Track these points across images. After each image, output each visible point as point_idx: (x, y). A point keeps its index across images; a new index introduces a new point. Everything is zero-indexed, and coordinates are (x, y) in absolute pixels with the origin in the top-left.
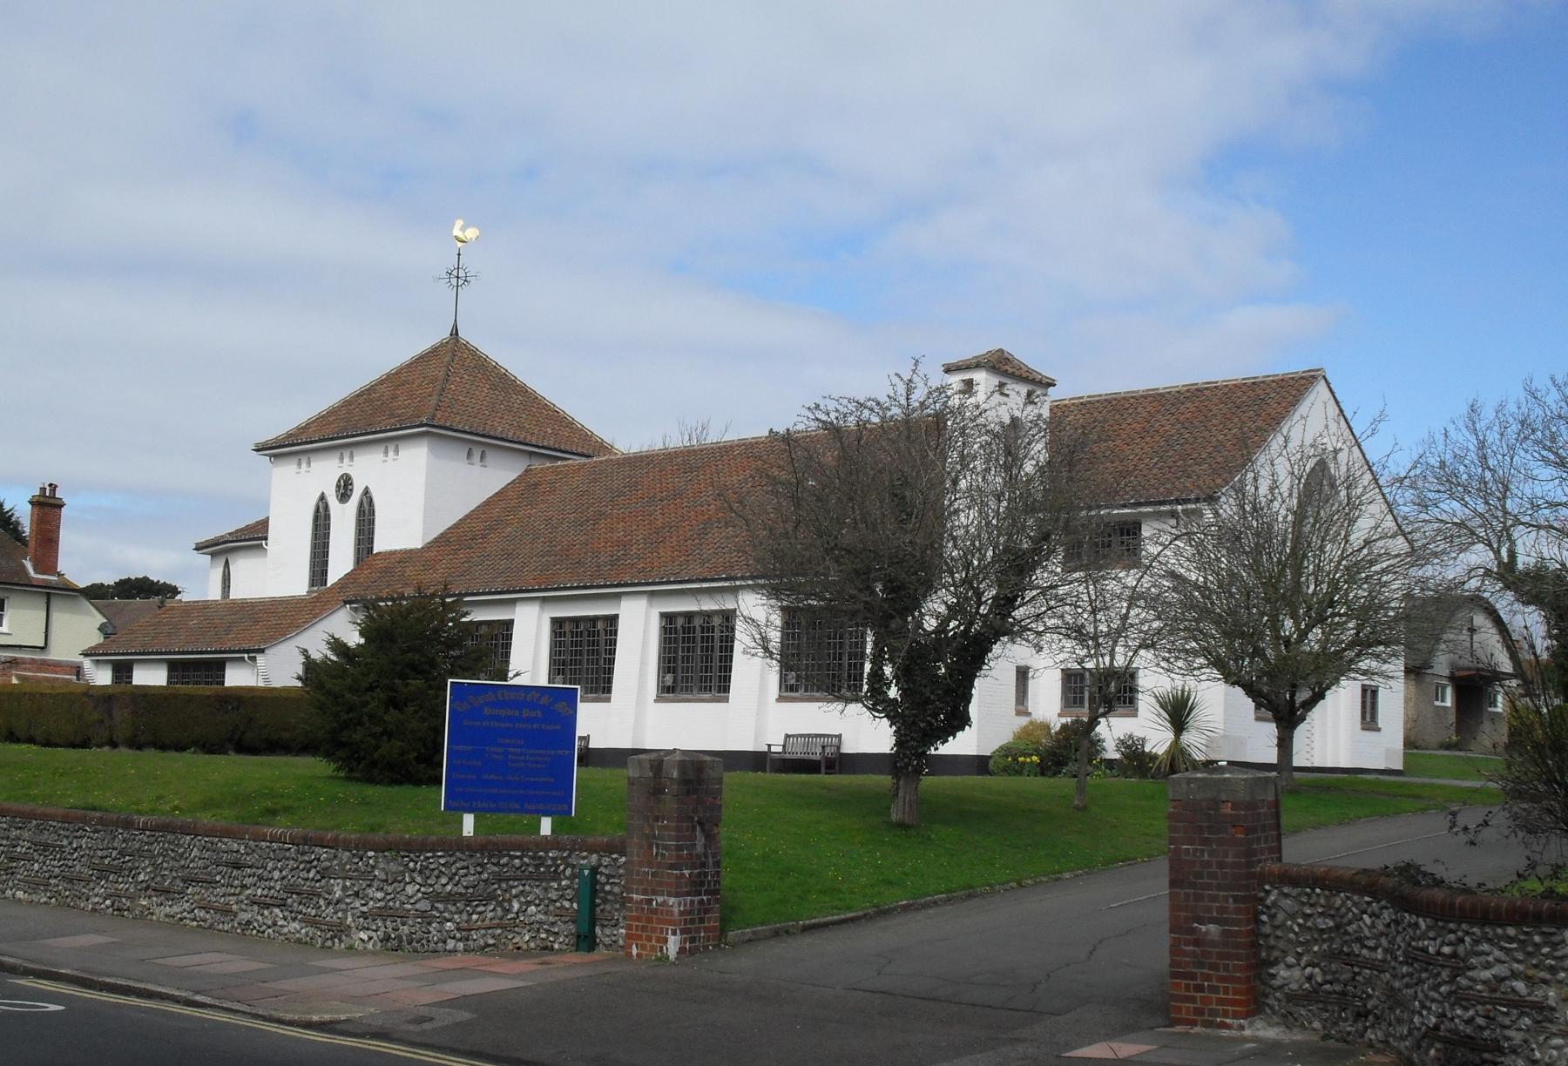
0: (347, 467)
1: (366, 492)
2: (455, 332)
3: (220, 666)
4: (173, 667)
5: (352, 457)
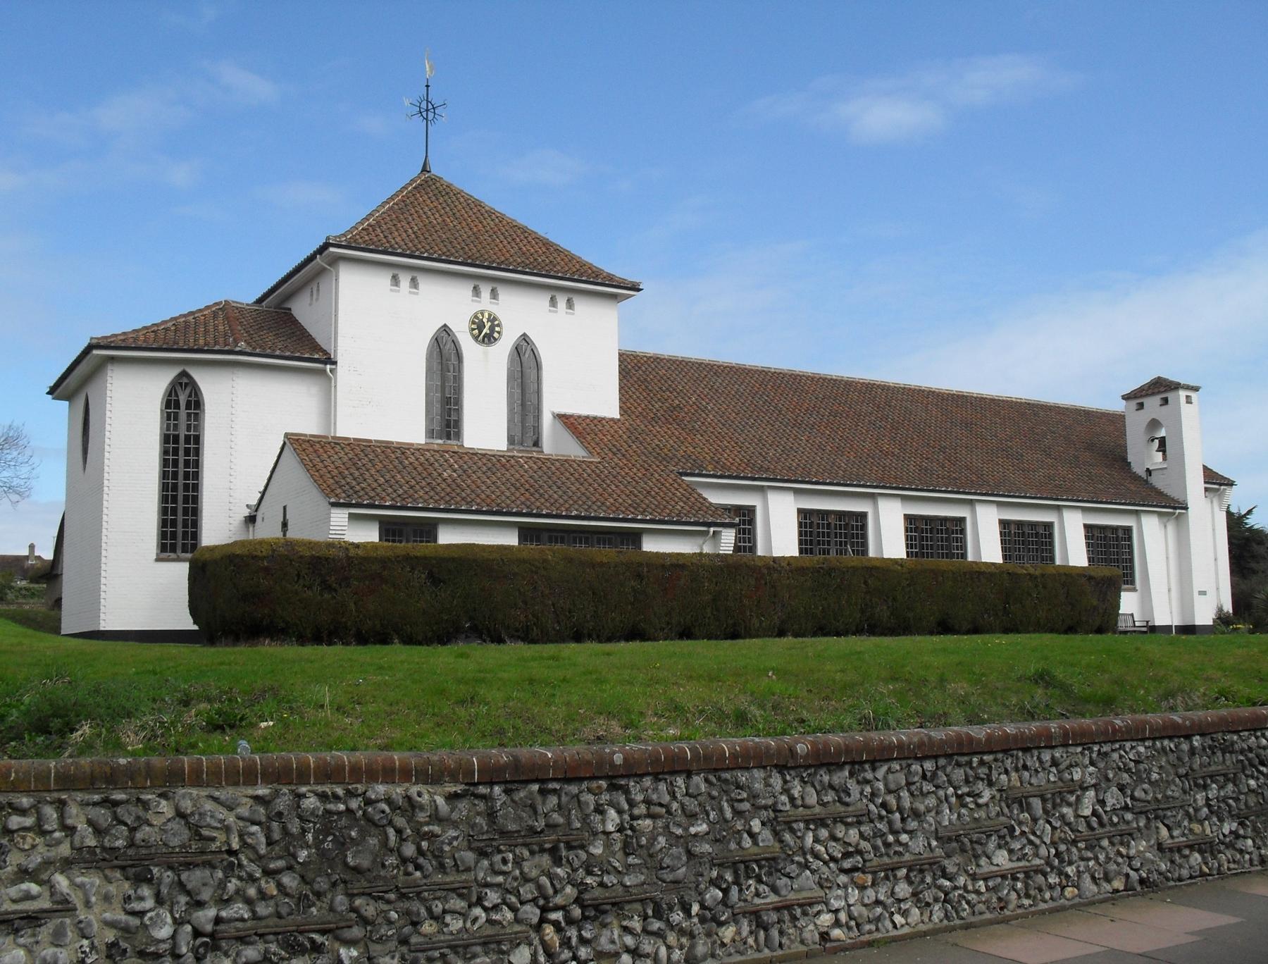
0: (485, 303)
1: (525, 337)
2: (425, 169)
3: (634, 537)
4: (527, 533)
5: (414, 283)
